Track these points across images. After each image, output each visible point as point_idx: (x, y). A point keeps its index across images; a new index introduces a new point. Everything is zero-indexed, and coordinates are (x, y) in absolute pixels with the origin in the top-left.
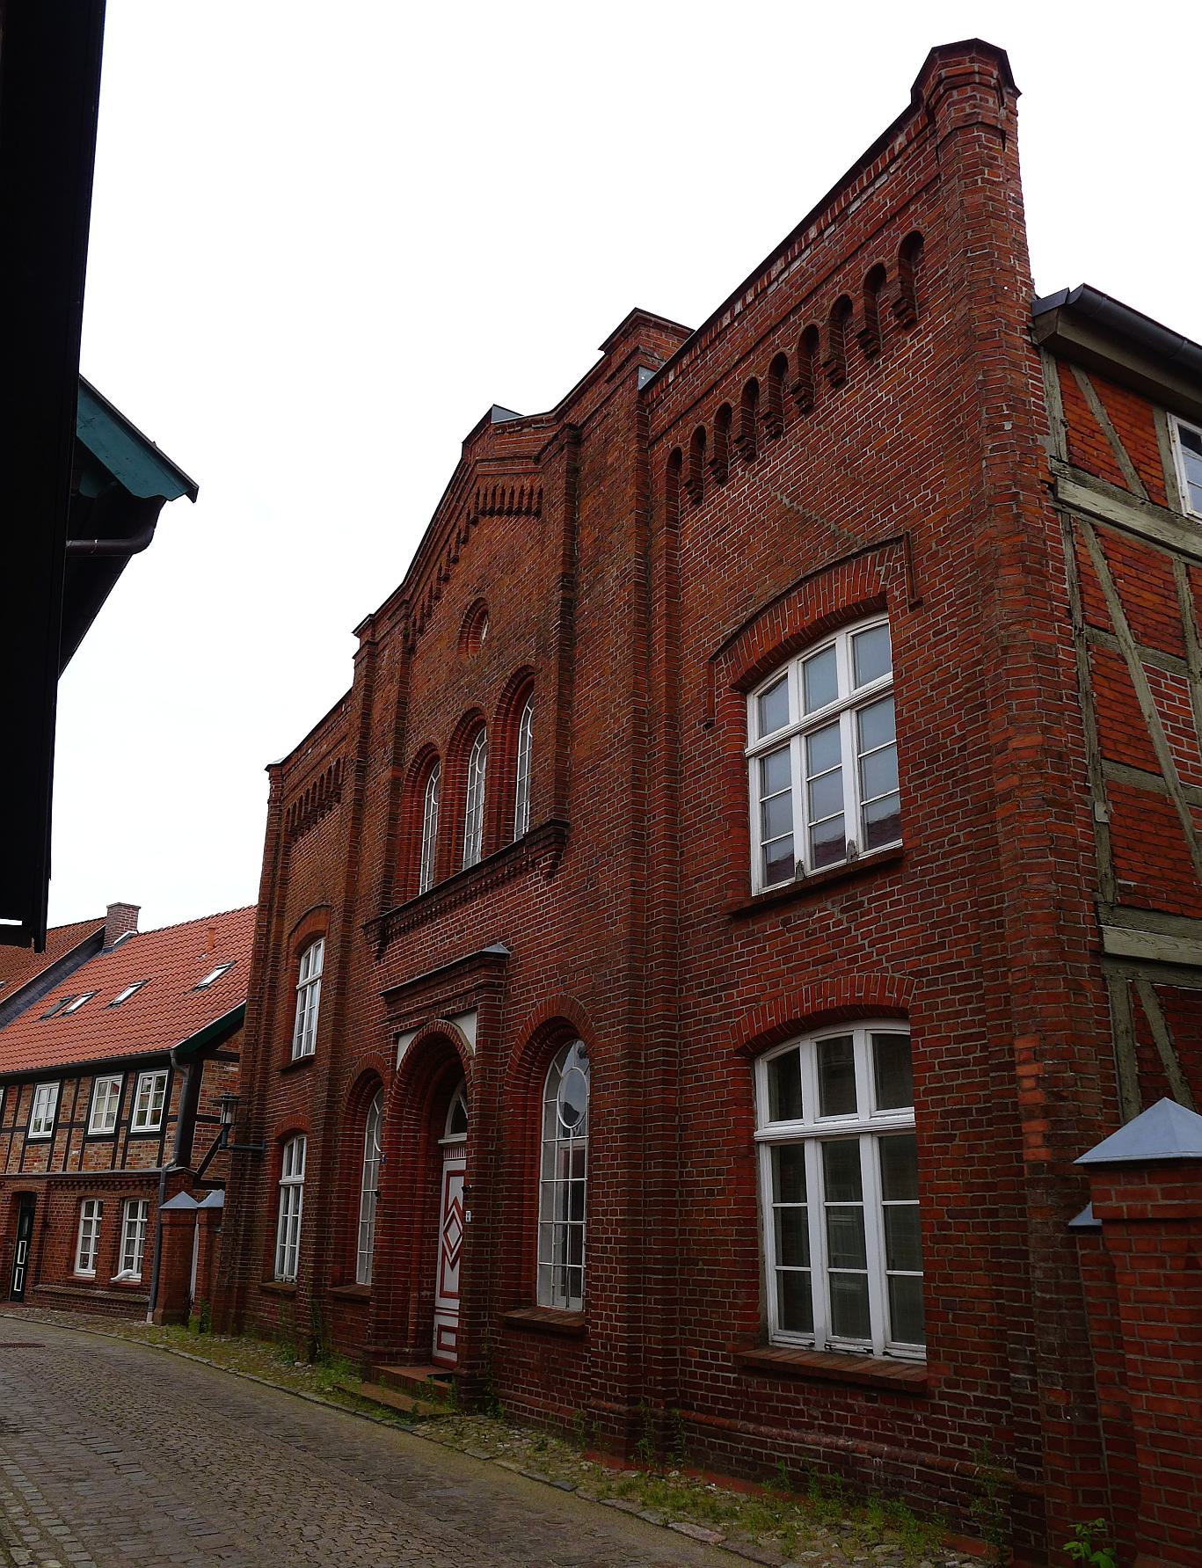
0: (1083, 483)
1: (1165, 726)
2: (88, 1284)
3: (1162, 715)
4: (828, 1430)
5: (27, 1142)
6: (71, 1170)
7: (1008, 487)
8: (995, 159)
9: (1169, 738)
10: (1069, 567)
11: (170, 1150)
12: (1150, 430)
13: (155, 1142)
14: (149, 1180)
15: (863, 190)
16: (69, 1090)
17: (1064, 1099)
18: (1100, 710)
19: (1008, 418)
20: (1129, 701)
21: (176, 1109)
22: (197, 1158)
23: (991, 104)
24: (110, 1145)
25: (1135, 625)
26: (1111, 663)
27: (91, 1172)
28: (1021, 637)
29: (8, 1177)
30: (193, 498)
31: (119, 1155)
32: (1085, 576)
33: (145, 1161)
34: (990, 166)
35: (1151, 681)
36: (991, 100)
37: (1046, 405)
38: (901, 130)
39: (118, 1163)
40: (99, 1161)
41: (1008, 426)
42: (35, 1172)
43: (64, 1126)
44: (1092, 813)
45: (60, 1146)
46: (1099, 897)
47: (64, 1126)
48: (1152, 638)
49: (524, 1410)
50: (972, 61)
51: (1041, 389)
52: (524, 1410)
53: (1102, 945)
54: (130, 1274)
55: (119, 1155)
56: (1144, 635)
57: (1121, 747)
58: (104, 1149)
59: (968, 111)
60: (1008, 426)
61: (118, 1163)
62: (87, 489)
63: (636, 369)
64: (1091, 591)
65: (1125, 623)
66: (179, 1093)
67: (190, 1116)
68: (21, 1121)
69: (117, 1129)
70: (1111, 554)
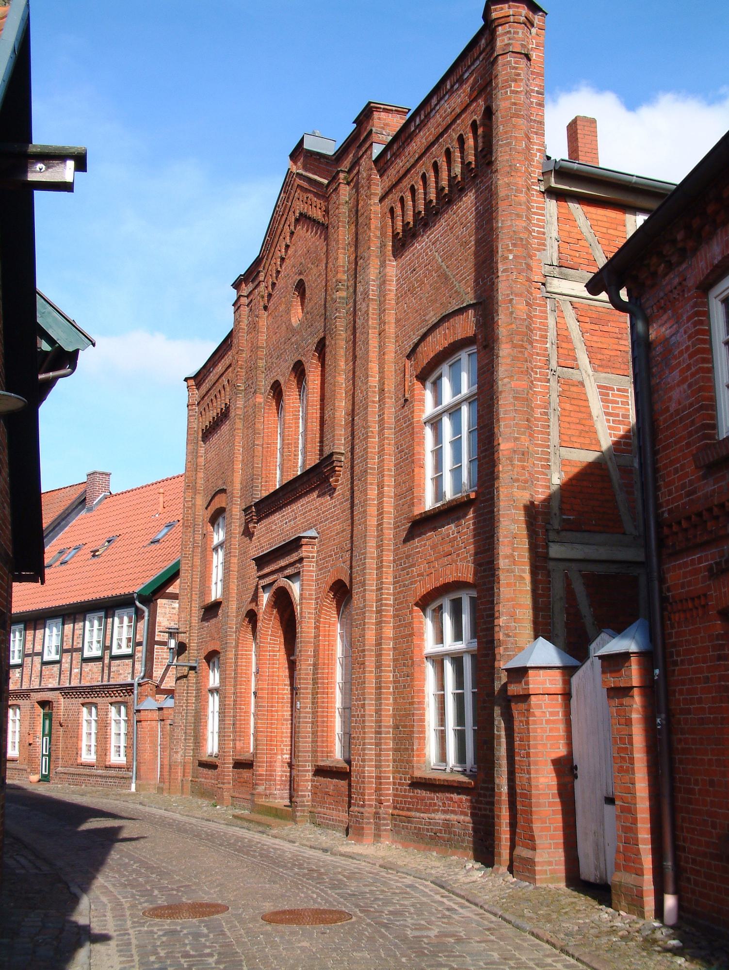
0: (565, 278)
1: (608, 421)
2: (91, 766)
3: (607, 414)
4: (445, 812)
5: (44, 663)
6: (75, 683)
7: (508, 295)
8: (519, 75)
9: (610, 428)
10: (552, 335)
11: (140, 668)
12: (621, 228)
13: (129, 662)
14: (128, 688)
15: (469, 67)
16: (68, 627)
17: (509, 636)
18: (562, 418)
19: (510, 251)
20: (583, 409)
21: (142, 636)
22: (158, 673)
23: (520, 35)
24: (99, 664)
25: (593, 361)
26: (573, 389)
27: (88, 684)
28: (509, 386)
29: (33, 690)
30: (94, 345)
31: (106, 671)
32: (563, 337)
33: (122, 674)
34: (515, 81)
35: (601, 394)
36: (520, 31)
37: (545, 230)
38: (483, 35)
39: (106, 677)
40: (93, 675)
41: (511, 257)
42: (50, 686)
43: (67, 651)
44: (549, 480)
45: (66, 665)
46: (549, 527)
47: (67, 651)
48: (608, 367)
49: (327, 819)
50: (509, 8)
51: (543, 221)
52: (327, 819)
53: (547, 553)
54: (117, 758)
55: (106, 671)
56: (599, 366)
57: (573, 439)
58: (96, 667)
59: (506, 42)
60: (511, 257)
61: (106, 677)
62: (45, 346)
63: (371, 144)
64: (564, 345)
65: (587, 361)
66: (143, 625)
67: (151, 642)
68: (38, 649)
69: (103, 653)
70: (581, 319)
